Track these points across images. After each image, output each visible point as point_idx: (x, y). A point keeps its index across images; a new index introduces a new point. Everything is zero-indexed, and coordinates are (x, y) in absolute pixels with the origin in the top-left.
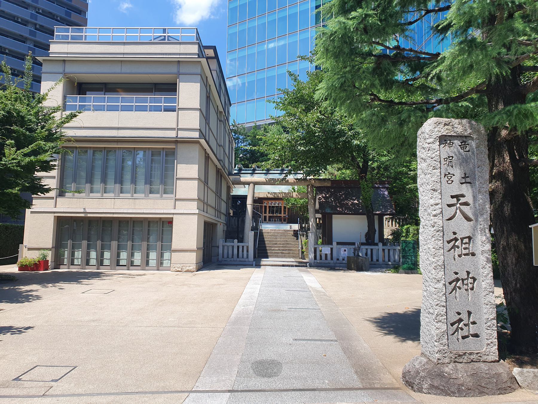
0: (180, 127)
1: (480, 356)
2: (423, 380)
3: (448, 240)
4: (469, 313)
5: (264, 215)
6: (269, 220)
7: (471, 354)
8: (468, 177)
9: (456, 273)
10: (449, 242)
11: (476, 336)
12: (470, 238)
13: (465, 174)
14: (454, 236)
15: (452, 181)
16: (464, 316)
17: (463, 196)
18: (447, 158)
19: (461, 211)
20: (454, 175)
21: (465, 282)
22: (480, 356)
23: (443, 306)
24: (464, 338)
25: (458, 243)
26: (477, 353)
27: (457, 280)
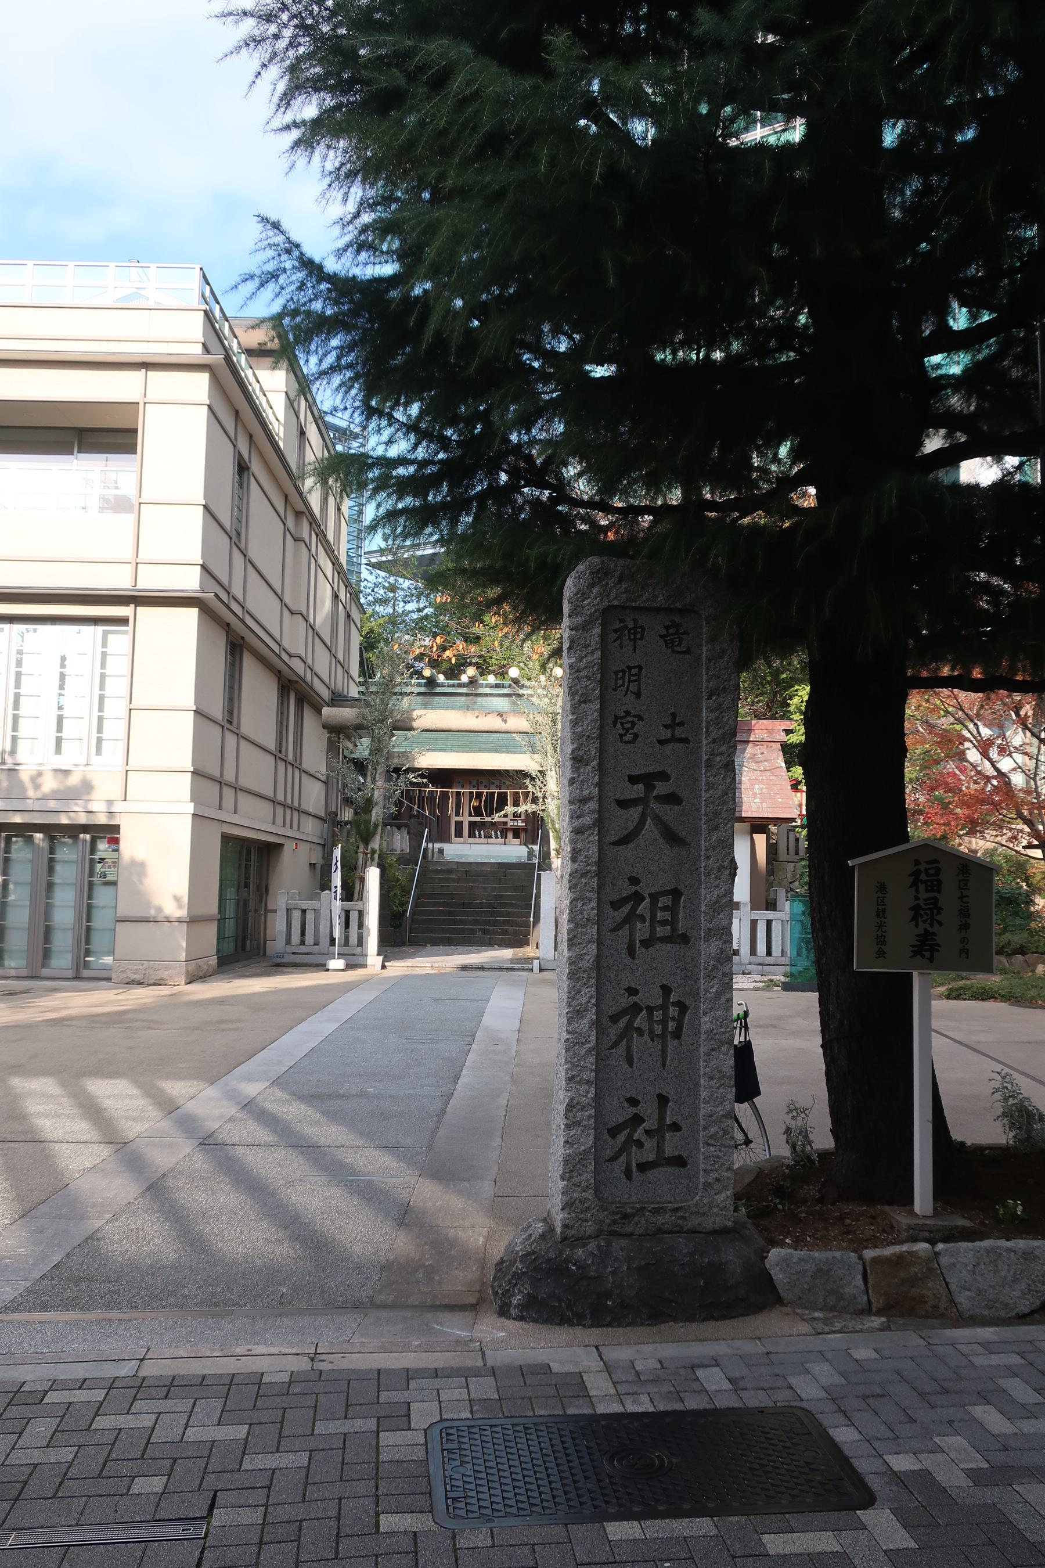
0: (129, 554)
1: (683, 1218)
2: (516, 1285)
3: (615, 897)
4: (663, 1100)
5: (455, 819)
6: (471, 835)
7: (657, 1211)
8: (681, 724)
9: (632, 991)
10: (616, 905)
11: (680, 1162)
12: (676, 894)
13: (674, 715)
14: (633, 889)
15: (636, 736)
16: (648, 1110)
17: (664, 776)
18: (623, 671)
19: (657, 818)
20: (641, 718)
21: (658, 1015)
22: (683, 1218)
23: (588, 1082)
24: (643, 1167)
25: (644, 907)
26: (677, 1210)
27: (636, 1008)
